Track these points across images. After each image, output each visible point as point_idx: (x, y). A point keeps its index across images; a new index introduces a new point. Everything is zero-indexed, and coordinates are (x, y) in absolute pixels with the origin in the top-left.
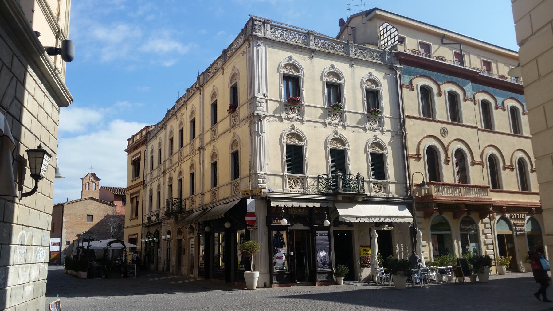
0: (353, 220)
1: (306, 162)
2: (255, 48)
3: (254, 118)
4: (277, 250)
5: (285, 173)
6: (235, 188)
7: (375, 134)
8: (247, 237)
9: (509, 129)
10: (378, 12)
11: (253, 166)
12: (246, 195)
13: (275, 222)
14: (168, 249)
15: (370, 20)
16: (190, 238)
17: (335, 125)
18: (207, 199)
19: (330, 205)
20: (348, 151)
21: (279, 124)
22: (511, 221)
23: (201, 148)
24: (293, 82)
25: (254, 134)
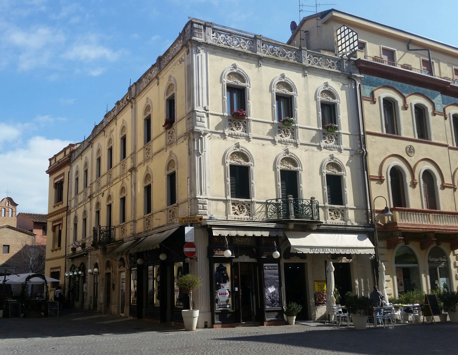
0: (306, 251)
3: (194, 135)
5: (229, 197)
6: (172, 214)
7: (331, 152)
8: (185, 270)
10: (335, 14)
11: (192, 189)
12: (184, 222)
13: (218, 254)
14: (95, 284)
15: (325, 23)
17: (286, 143)
20: (300, 172)
21: (222, 141)
23: (133, 169)
24: (238, 94)
25: (194, 153)
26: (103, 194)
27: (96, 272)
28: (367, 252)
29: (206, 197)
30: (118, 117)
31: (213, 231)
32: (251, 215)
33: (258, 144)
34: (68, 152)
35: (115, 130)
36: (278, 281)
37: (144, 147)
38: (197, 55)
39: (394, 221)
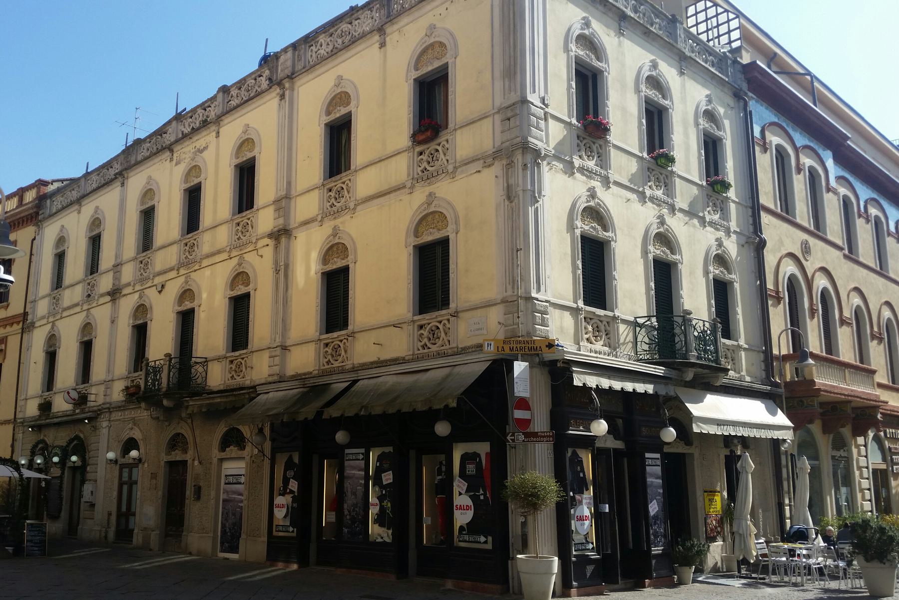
1: (615, 282)
4: (573, 498)
9: (873, 261)
12: (507, 351)
14: (127, 486)
16: (221, 460)
18: (304, 360)
19: (671, 390)
21: (569, 181)
22: (886, 442)
23: (281, 235)
25: (518, 199)
26: (163, 286)
27: (134, 459)
30: (226, 121)
31: (574, 375)
33: (620, 197)
34: (30, 196)
35: (212, 149)
36: (363, 482)
37: (323, 185)
39: (808, 377)
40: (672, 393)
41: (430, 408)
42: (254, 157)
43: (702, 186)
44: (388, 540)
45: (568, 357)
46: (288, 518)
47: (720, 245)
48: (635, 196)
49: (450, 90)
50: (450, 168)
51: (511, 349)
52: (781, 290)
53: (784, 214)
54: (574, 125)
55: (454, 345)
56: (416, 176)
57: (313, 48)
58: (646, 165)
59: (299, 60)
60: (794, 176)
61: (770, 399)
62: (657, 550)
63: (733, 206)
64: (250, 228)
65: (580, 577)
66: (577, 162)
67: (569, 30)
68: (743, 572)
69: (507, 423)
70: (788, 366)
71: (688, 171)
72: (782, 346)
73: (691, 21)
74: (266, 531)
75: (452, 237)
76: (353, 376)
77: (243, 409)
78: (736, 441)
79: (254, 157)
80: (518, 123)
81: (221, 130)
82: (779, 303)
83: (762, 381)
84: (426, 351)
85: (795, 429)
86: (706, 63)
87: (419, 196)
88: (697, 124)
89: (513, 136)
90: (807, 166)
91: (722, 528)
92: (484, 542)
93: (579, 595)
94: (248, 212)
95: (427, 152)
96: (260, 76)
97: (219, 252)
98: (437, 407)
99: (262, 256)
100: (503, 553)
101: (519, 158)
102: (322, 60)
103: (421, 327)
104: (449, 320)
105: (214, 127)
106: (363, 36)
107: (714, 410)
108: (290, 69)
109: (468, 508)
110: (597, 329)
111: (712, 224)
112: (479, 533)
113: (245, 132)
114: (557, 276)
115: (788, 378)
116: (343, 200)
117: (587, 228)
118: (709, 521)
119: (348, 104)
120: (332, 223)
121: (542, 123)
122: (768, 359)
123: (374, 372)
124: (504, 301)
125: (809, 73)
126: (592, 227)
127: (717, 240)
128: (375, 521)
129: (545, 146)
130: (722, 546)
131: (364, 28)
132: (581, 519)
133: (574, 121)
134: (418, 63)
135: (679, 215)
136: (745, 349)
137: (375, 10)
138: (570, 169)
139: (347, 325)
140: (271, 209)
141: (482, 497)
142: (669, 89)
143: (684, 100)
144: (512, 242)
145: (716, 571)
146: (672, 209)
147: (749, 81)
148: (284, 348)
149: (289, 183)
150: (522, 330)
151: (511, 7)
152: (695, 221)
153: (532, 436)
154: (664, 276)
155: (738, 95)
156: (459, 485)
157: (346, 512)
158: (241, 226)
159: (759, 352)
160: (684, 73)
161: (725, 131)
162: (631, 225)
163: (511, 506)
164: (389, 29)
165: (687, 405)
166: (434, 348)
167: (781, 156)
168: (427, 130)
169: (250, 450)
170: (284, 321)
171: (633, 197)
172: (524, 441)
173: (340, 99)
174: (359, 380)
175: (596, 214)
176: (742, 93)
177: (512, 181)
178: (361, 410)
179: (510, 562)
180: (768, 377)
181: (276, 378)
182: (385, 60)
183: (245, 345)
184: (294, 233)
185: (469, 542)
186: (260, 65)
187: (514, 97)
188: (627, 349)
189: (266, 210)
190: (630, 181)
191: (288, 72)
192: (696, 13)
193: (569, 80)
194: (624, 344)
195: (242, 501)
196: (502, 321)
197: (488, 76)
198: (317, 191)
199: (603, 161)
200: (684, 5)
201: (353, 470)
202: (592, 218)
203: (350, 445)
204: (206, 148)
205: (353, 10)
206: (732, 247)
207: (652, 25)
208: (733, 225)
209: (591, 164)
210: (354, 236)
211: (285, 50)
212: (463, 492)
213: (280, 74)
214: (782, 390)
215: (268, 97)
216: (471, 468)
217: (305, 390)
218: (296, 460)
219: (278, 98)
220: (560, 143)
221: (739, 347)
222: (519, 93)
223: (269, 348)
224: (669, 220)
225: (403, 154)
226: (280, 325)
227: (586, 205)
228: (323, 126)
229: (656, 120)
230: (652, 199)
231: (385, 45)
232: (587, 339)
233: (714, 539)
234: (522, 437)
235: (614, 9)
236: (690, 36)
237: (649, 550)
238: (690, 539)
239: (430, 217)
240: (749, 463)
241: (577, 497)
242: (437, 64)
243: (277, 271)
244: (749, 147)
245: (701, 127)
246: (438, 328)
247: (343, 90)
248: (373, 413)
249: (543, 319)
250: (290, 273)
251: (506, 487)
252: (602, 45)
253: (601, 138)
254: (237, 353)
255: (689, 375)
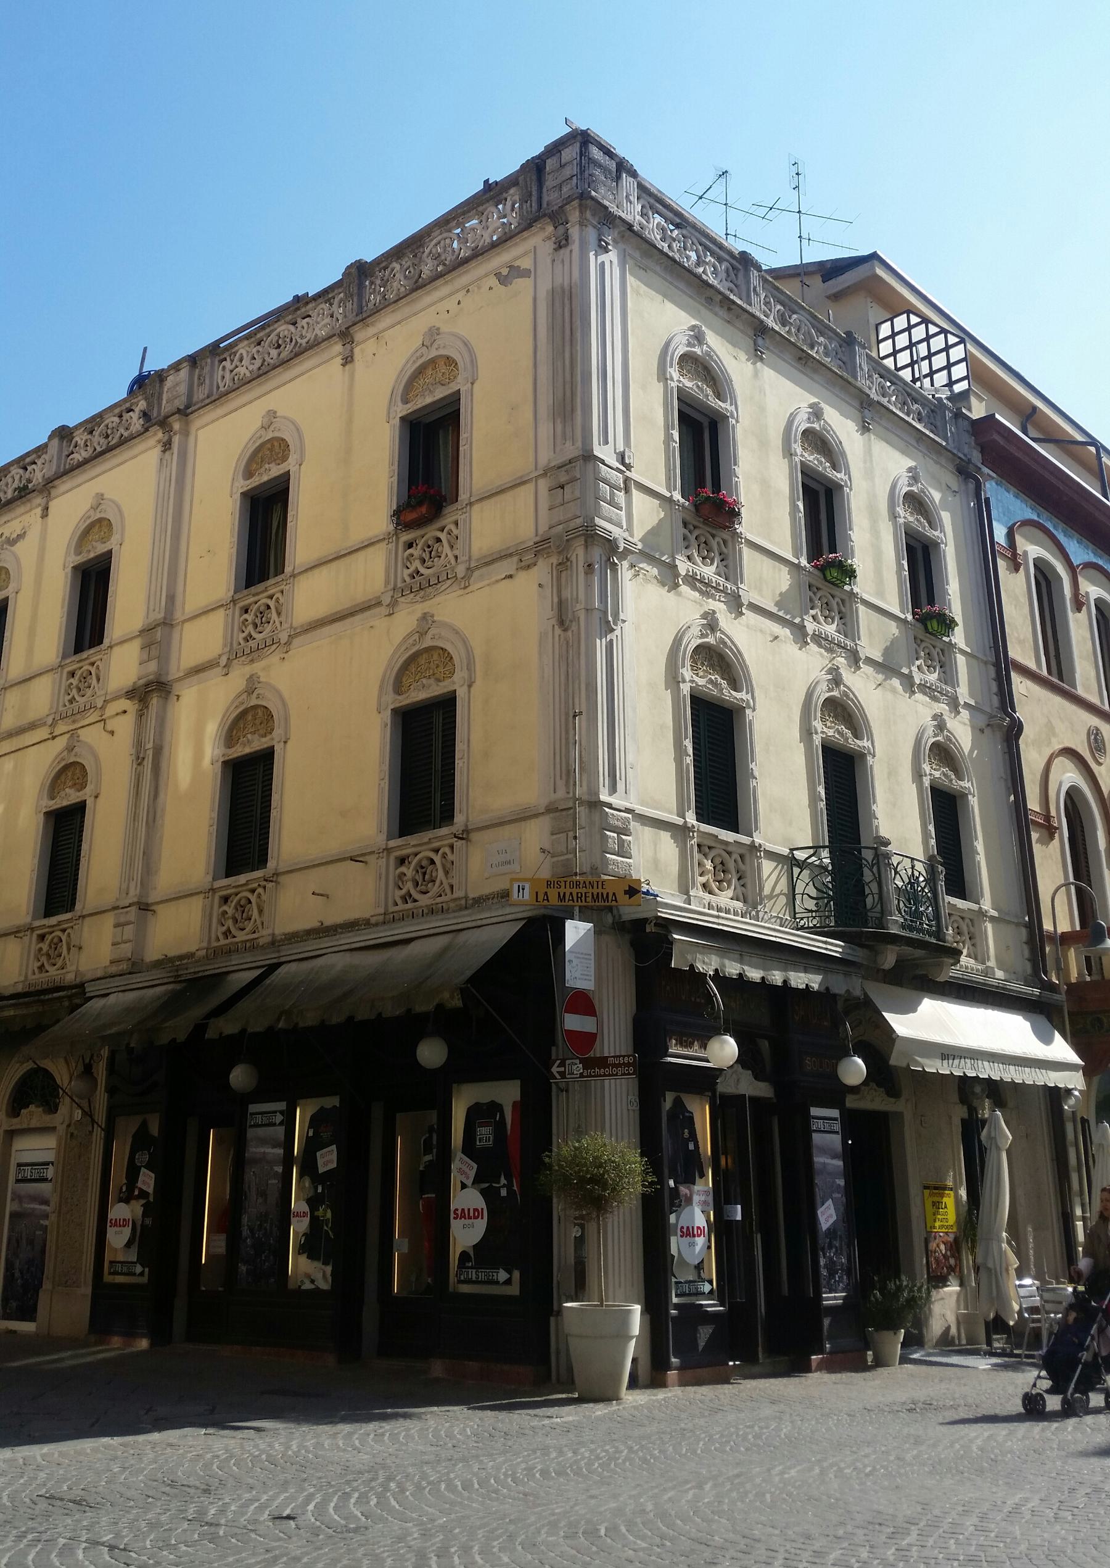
0: (934, 1066)
2: (592, 254)
4: (675, 1192)
10: (880, 272)
12: (554, 900)
13: (678, 1054)
15: (836, 297)
16: (11, 1134)
18: (180, 930)
23: (152, 692)
25: (579, 626)
28: (1054, 1079)
29: (629, 805)
30: (63, 488)
32: (750, 899)
36: (279, 1169)
37: (234, 601)
38: (601, 258)
40: (857, 992)
41: (409, 1011)
42: (110, 552)
43: (905, 621)
44: (325, 1286)
45: (665, 913)
46: (134, 1250)
47: (941, 726)
48: (788, 631)
49: (463, 436)
50: (461, 570)
51: (562, 898)
52: (1053, 813)
53: (1055, 680)
54: (676, 503)
55: (461, 894)
56: (399, 585)
57: (227, 364)
58: (806, 580)
59: (201, 384)
60: (1070, 614)
61: (1041, 1013)
62: (832, 1298)
63: (961, 660)
64: (94, 681)
65: (686, 1348)
66: (683, 566)
67: (667, 344)
68: (996, 1345)
69: (554, 1043)
70: (1072, 953)
71: (881, 594)
72: (1060, 916)
73: (886, 348)
74: (90, 1275)
75: (461, 693)
76: (270, 958)
77: (56, 1027)
78: (978, 1089)
79: (110, 552)
80: (577, 494)
81: (52, 504)
82: (1052, 837)
83: (1025, 981)
84: (410, 905)
85: (1088, 1072)
86: (908, 415)
87: (406, 620)
88: (894, 516)
89: (570, 515)
90: (1092, 597)
91: (959, 1259)
92: (506, 1282)
93: (683, 1383)
94: (92, 651)
95: (421, 543)
96: (130, 410)
97: (32, 726)
98: (420, 1008)
99: (112, 733)
100: (540, 1303)
101: (579, 554)
102: (241, 384)
103: (402, 861)
104: (452, 847)
105: (39, 500)
106: (315, 344)
107: (933, 1024)
108: (184, 399)
109: (477, 1214)
110: (721, 867)
111: (925, 688)
112: (495, 1266)
113: (95, 508)
114: (648, 769)
115: (1074, 976)
116: (268, 628)
117: (701, 682)
118: (933, 1246)
119: (285, 458)
120: (248, 670)
121: (620, 497)
122: (1036, 939)
123: (311, 946)
124: (551, 809)
125: (1094, 442)
126: (711, 681)
127: (935, 717)
128: (301, 1249)
129: (626, 535)
130: (959, 1294)
131: (317, 331)
132: (689, 1233)
133: (677, 496)
134: (408, 391)
135: (866, 669)
136: (992, 919)
137: (337, 300)
138: (670, 578)
139: (266, 861)
140: (136, 645)
141: (504, 1192)
142: (843, 454)
143: (869, 474)
144: (567, 702)
145: (946, 1343)
146: (854, 659)
147: (984, 449)
148: (145, 907)
149: (171, 598)
150: (582, 862)
151: (567, 302)
152: (896, 682)
153: (598, 1065)
154: (842, 776)
155: (964, 471)
156: (462, 1169)
157: (245, 1232)
158: (77, 677)
159: (1017, 924)
160: (869, 430)
161: (943, 531)
162: (781, 680)
163: (558, 1207)
164: (359, 335)
165: (888, 1016)
166: (424, 901)
167: (1045, 582)
168: (420, 504)
169: (67, 1112)
170: (147, 854)
171: (785, 633)
172: (582, 1075)
173: (271, 450)
174: (278, 965)
175: (717, 658)
176: (971, 469)
177: (567, 594)
178: (279, 1020)
179: (552, 1319)
180: (1036, 972)
181: (124, 966)
182: (351, 387)
183: (69, 903)
184: (177, 689)
185: (477, 1282)
186: (131, 391)
187: (571, 450)
188: (778, 907)
189: (126, 646)
190: (776, 604)
191: (180, 403)
192: (893, 335)
193: (667, 428)
194: (770, 897)
195: (46, 1216)
196: (547, 847)
197: (529, 415)
198: (221, 613)
199: (731, 568)
200: (873, 322)
201: (263, 1147)
202: (712, 666)
203: (260, 1094)
204: (21, 537)
205: (300, 301)
206: (962, 732)
207: (812, 348)
208: (963, 693)
209: (708, 571)
210: (286, 694)
211: (176, 367)
212: (469, 1182)
213: (166, 407)
214: (1061, 997)
215: (141, 447)
216: (485, 1134)
217: (178, 987)
218: (154, 1129)
219: (159, 448)
220: (653, 532)
221: (982, 913)
222: (579, 444)
223: (115, 908)
224: (849, 677)
225: (377, 546)
226: (139, 864)
227: (700, 641)
228: (238, 496)
229: (821, 505)
230: (818, 639)
231: (352, 360)
232: (705, 886)
233: (939, 1281)
234: (578, 1068)
235: (746, 315)
236: (876, 364)
237: (818, 1298)
238: (897, 1275)
239: (423, 657)
240: (1002, 1131)
241: (683, 1190)
242: (440, 393)
243: (139, 760)
244: (985, 560)
245: (902, 521)
246: (432, 862)
247: (277, 434)
248: (301, 1025)
249: (621, 843)
250: (164, 765)
251: (549, 1167)
252: (724, 372)
253: (725, 527)
254: (53, 920)
255: (889, 958)
